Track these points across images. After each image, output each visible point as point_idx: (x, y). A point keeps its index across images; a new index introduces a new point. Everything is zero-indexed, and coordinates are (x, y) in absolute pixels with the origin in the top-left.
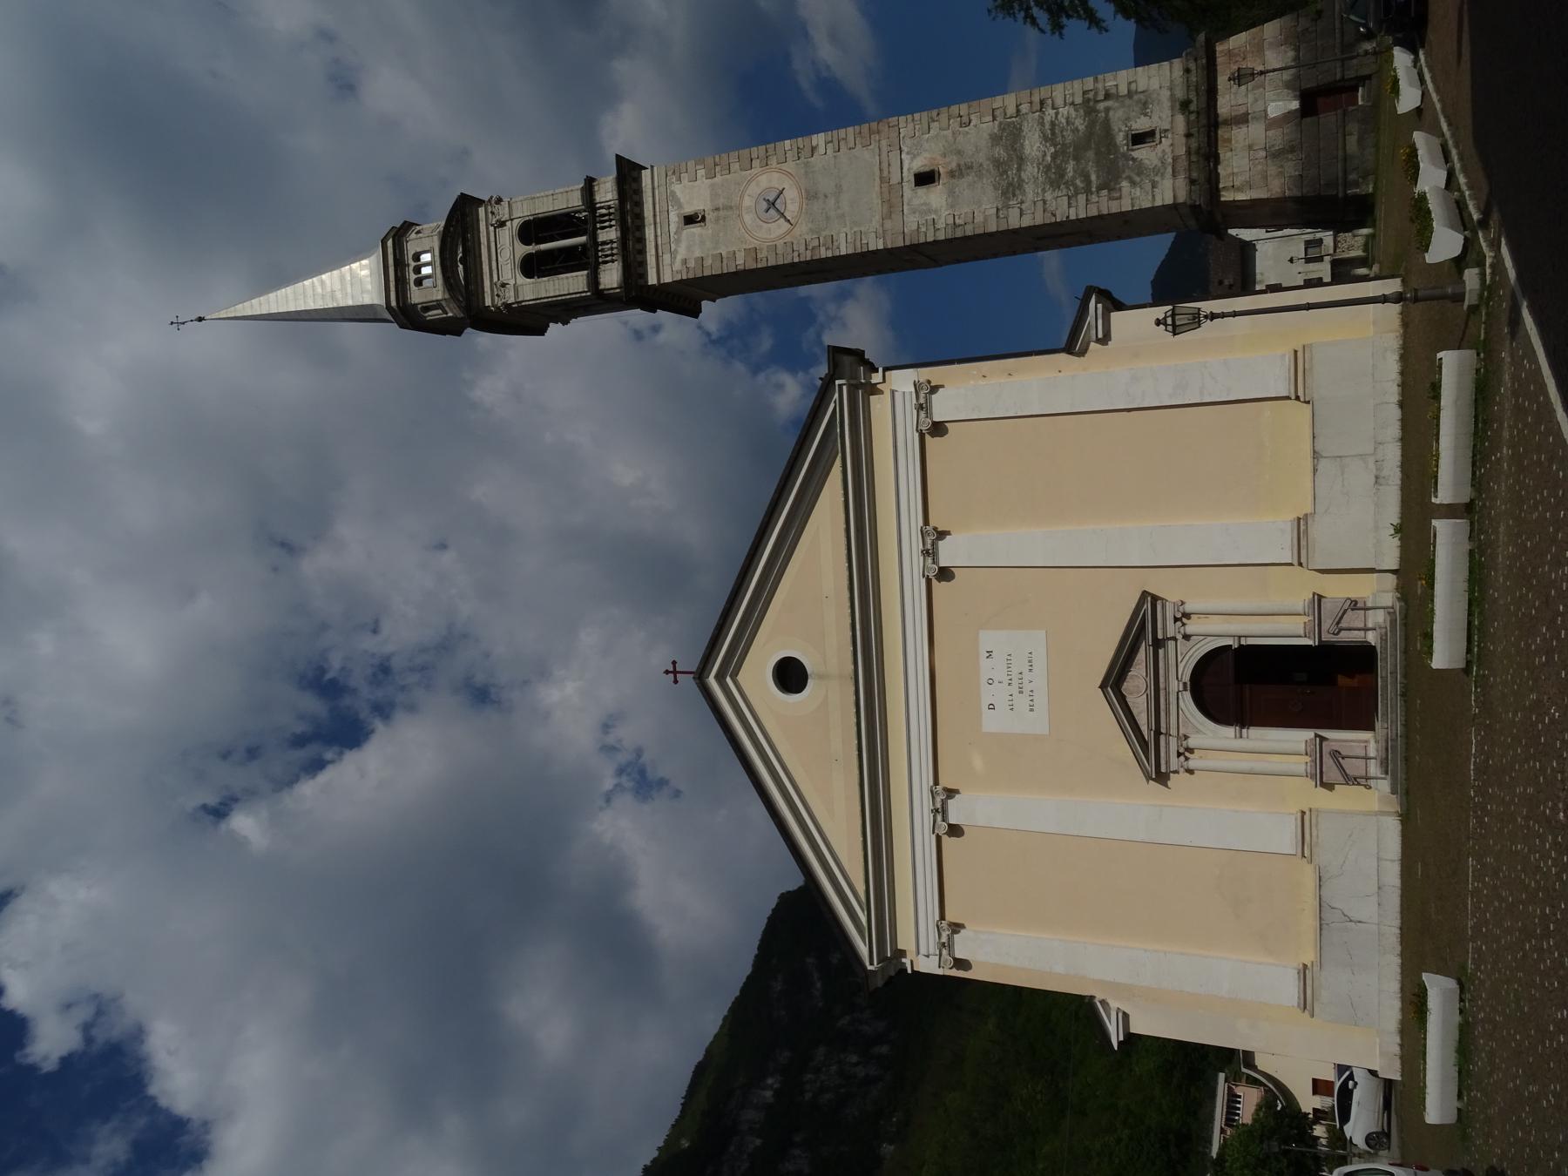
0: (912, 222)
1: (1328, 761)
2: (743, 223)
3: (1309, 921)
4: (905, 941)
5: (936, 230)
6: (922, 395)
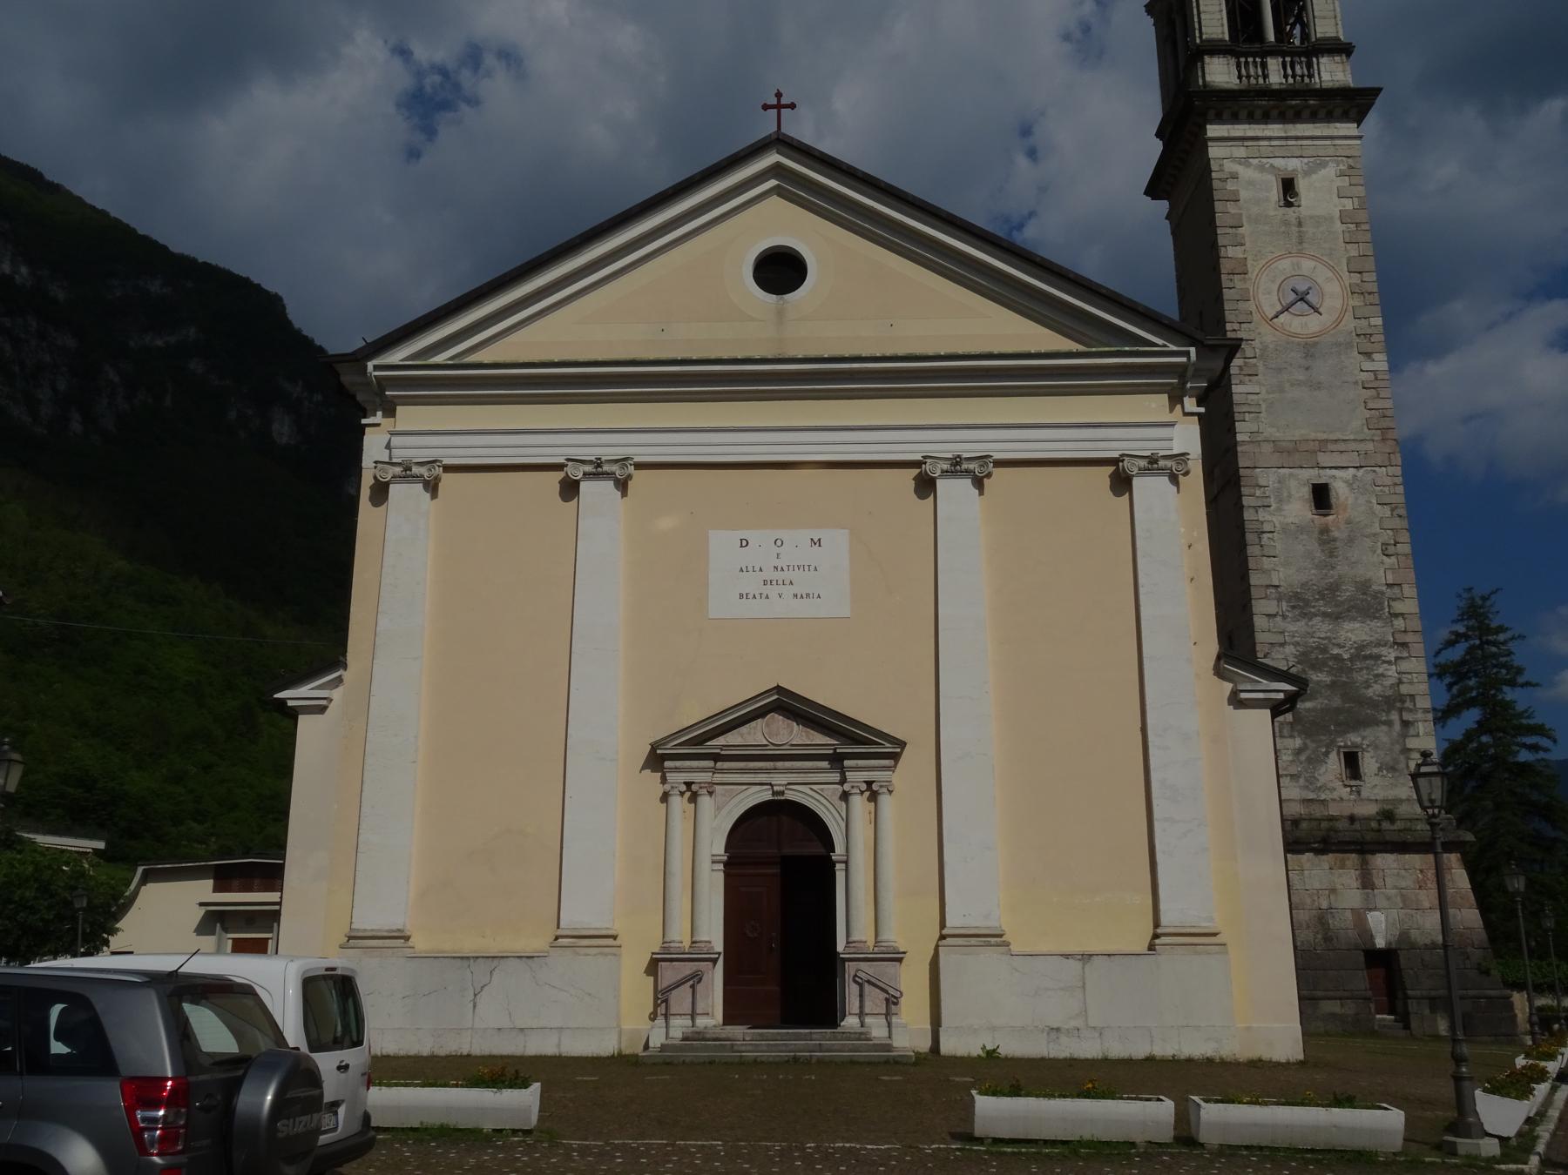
0: (1268, 478)
1: (688, 969)
2: (1281, 258)
3: (469, 944)
4: (408, 417)
5: (1256, 508)
6: (1169, 463)
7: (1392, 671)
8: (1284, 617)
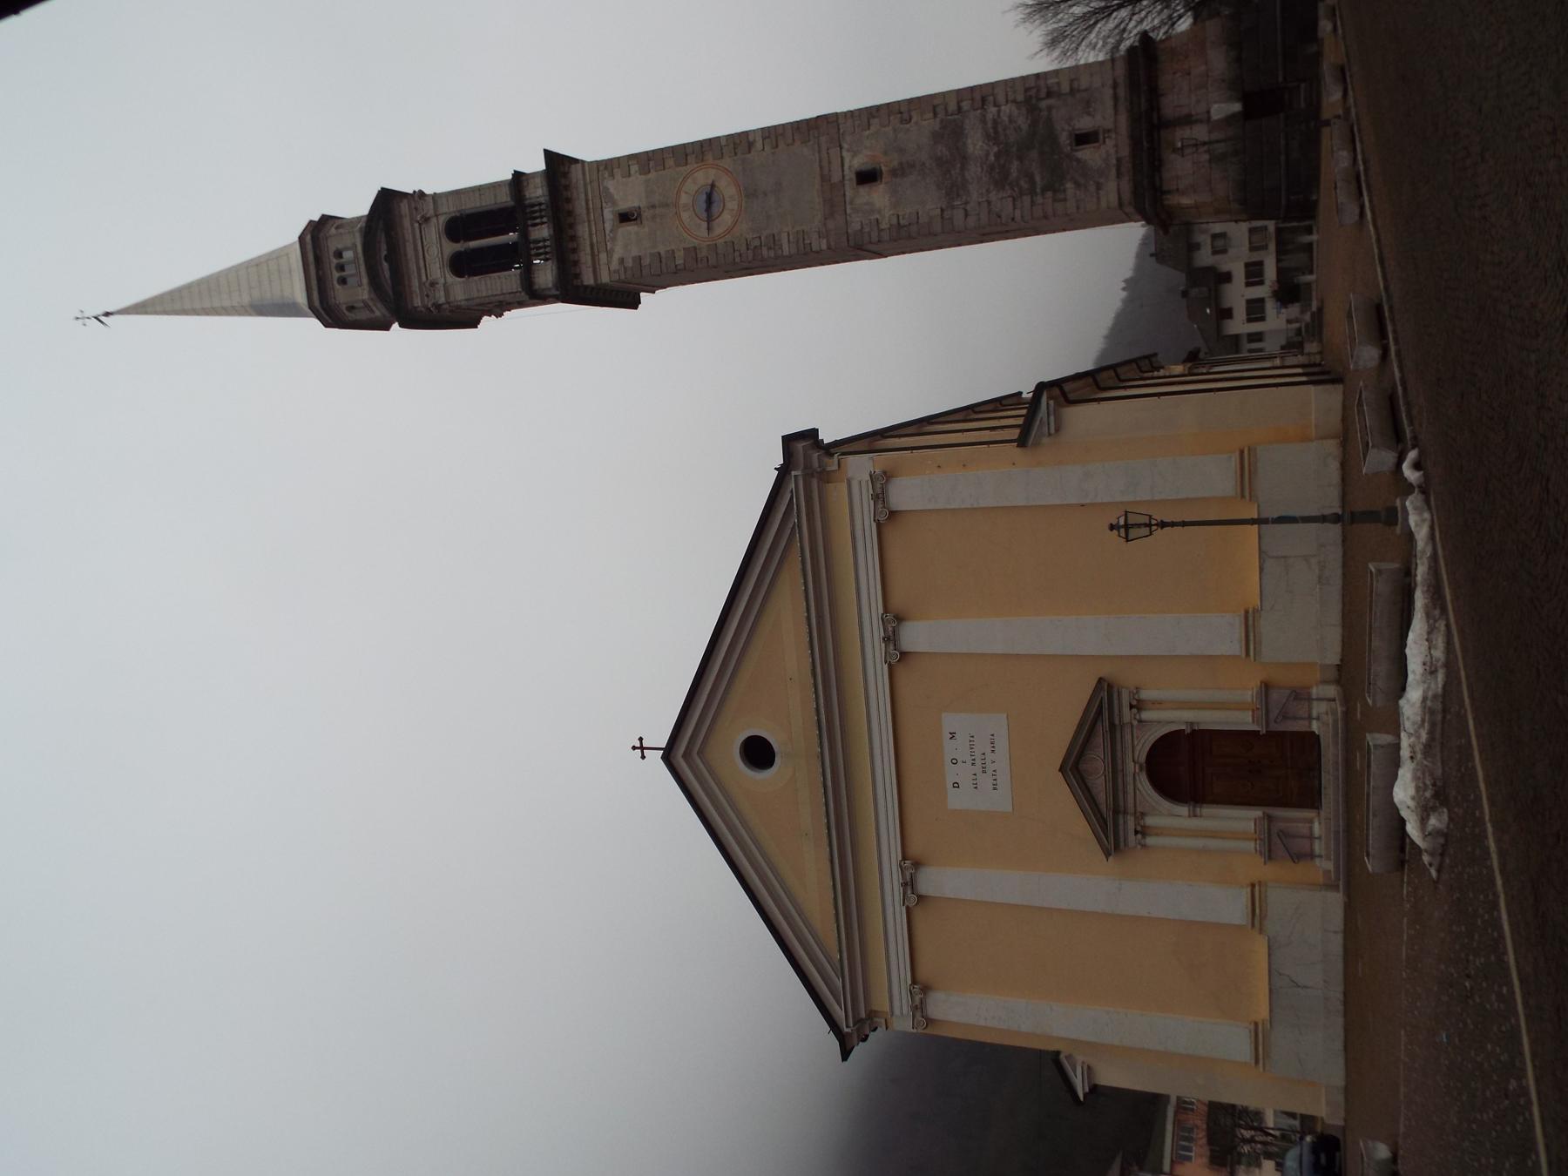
7: (1005, 109)
8: (967, 203)
